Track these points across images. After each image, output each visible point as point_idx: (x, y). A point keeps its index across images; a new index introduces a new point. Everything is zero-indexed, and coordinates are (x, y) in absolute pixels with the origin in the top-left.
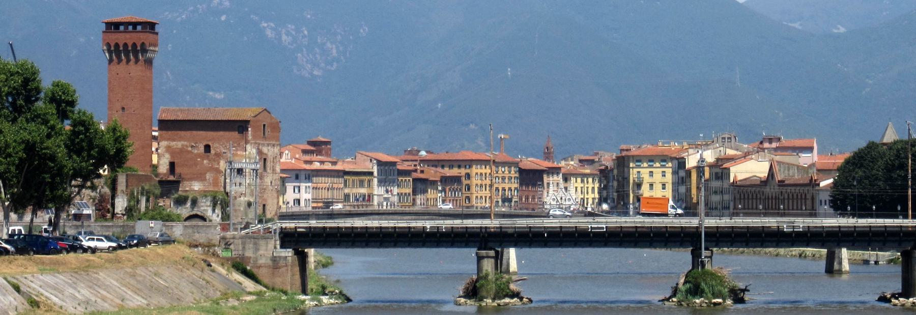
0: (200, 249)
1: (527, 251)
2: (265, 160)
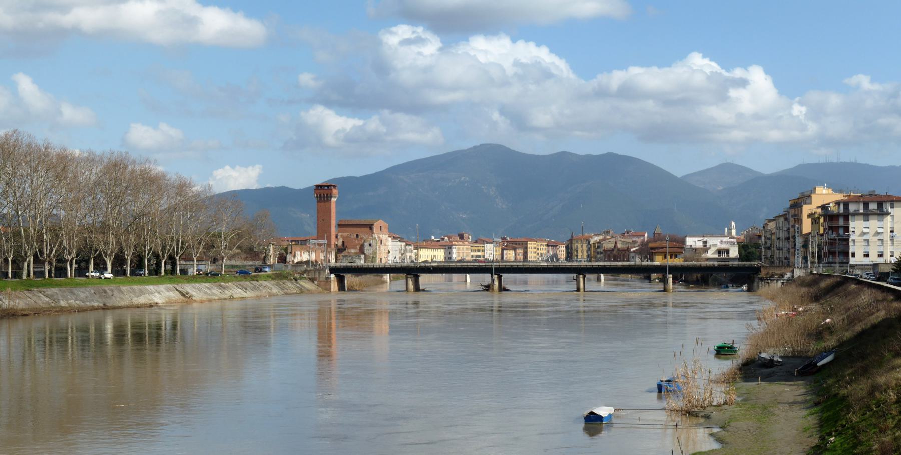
0: (751, 423)
1: (471, 275)
2: (381, 240)
